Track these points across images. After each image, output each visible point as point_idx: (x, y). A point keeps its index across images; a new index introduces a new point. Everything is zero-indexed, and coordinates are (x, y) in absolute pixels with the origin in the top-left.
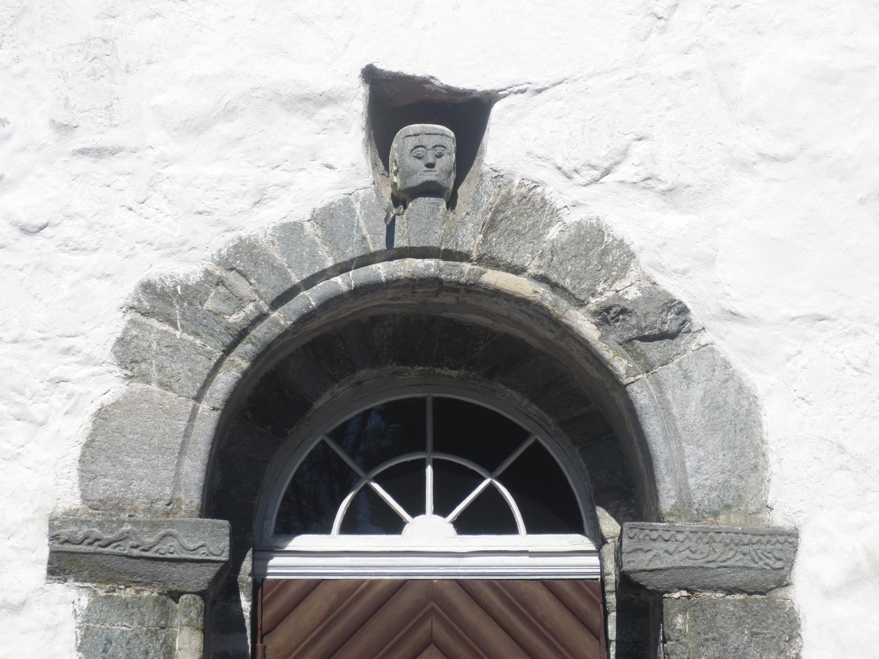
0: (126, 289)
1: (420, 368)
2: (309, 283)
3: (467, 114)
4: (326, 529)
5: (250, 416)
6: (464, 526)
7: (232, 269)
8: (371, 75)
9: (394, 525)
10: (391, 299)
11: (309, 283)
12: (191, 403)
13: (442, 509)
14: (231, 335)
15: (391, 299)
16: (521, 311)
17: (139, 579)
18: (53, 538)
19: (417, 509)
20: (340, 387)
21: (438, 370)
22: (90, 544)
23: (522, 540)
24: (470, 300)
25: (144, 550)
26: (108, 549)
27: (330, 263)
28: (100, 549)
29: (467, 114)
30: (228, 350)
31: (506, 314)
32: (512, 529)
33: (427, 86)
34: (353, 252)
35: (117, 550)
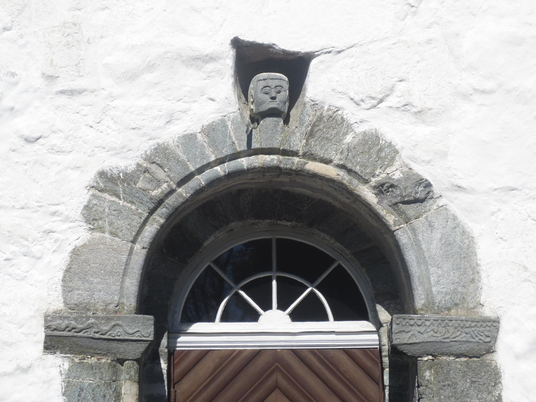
0: (89, 176)
1: (268, 221)
2: (200, 170)
3: (295, 67)
4: (212, 319)
5: (165, 251)
6: (296, 316)
7: (153, 163)
8: (236, 43)
9: (254, 317)
10: (250, 179)
11: (200, 170)
12: (130, 244)
13: (282, 306)
14: (153, 203)
15: (250, 179)
16: (329, 186)
17: (99, 352)
18: (47, 327)
19: (267, 306)
20: (219, 233)
21: (279, 222)
22: (70, 331)
23: (331, 324)
24: (298, 179)
25: (102, 334)
26: (81, 334)
27: (213, 158)
28: (76, 334)
29: (295, 67)
30: (152, 212)
31: (320, 188)
32: (326, 319)
33: (271, 50)
34: (227, 151)
35: (86, 335)
